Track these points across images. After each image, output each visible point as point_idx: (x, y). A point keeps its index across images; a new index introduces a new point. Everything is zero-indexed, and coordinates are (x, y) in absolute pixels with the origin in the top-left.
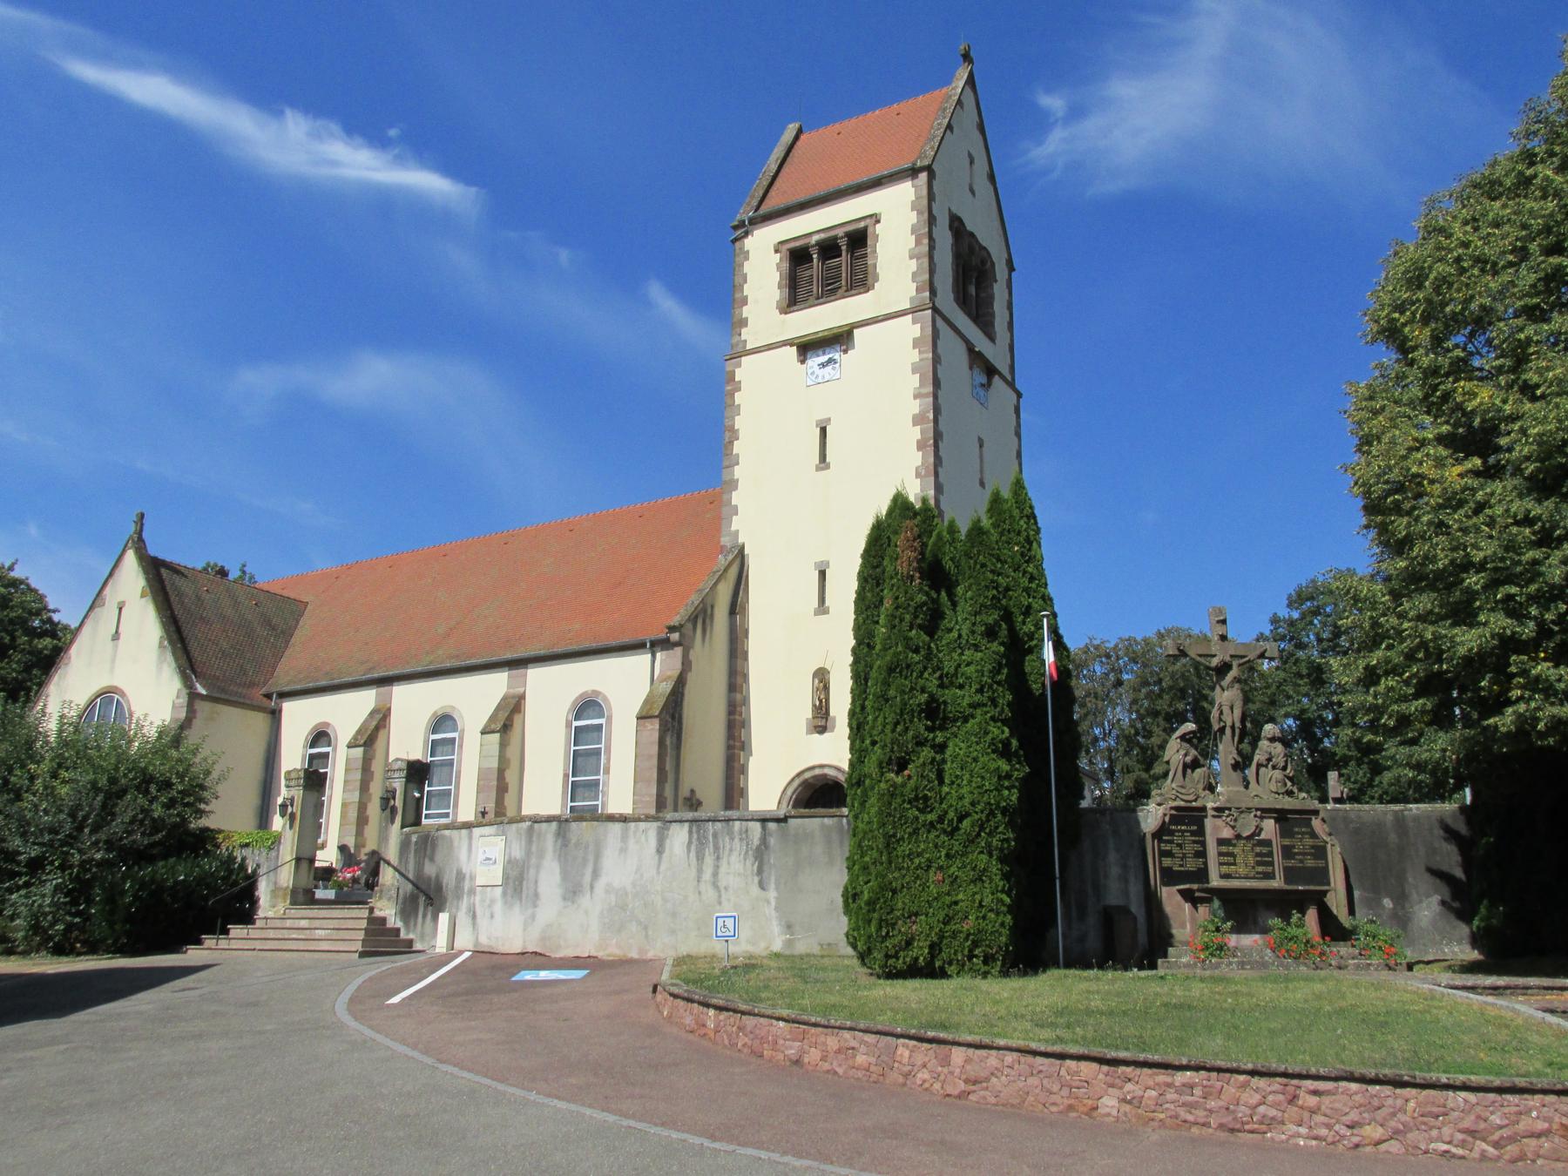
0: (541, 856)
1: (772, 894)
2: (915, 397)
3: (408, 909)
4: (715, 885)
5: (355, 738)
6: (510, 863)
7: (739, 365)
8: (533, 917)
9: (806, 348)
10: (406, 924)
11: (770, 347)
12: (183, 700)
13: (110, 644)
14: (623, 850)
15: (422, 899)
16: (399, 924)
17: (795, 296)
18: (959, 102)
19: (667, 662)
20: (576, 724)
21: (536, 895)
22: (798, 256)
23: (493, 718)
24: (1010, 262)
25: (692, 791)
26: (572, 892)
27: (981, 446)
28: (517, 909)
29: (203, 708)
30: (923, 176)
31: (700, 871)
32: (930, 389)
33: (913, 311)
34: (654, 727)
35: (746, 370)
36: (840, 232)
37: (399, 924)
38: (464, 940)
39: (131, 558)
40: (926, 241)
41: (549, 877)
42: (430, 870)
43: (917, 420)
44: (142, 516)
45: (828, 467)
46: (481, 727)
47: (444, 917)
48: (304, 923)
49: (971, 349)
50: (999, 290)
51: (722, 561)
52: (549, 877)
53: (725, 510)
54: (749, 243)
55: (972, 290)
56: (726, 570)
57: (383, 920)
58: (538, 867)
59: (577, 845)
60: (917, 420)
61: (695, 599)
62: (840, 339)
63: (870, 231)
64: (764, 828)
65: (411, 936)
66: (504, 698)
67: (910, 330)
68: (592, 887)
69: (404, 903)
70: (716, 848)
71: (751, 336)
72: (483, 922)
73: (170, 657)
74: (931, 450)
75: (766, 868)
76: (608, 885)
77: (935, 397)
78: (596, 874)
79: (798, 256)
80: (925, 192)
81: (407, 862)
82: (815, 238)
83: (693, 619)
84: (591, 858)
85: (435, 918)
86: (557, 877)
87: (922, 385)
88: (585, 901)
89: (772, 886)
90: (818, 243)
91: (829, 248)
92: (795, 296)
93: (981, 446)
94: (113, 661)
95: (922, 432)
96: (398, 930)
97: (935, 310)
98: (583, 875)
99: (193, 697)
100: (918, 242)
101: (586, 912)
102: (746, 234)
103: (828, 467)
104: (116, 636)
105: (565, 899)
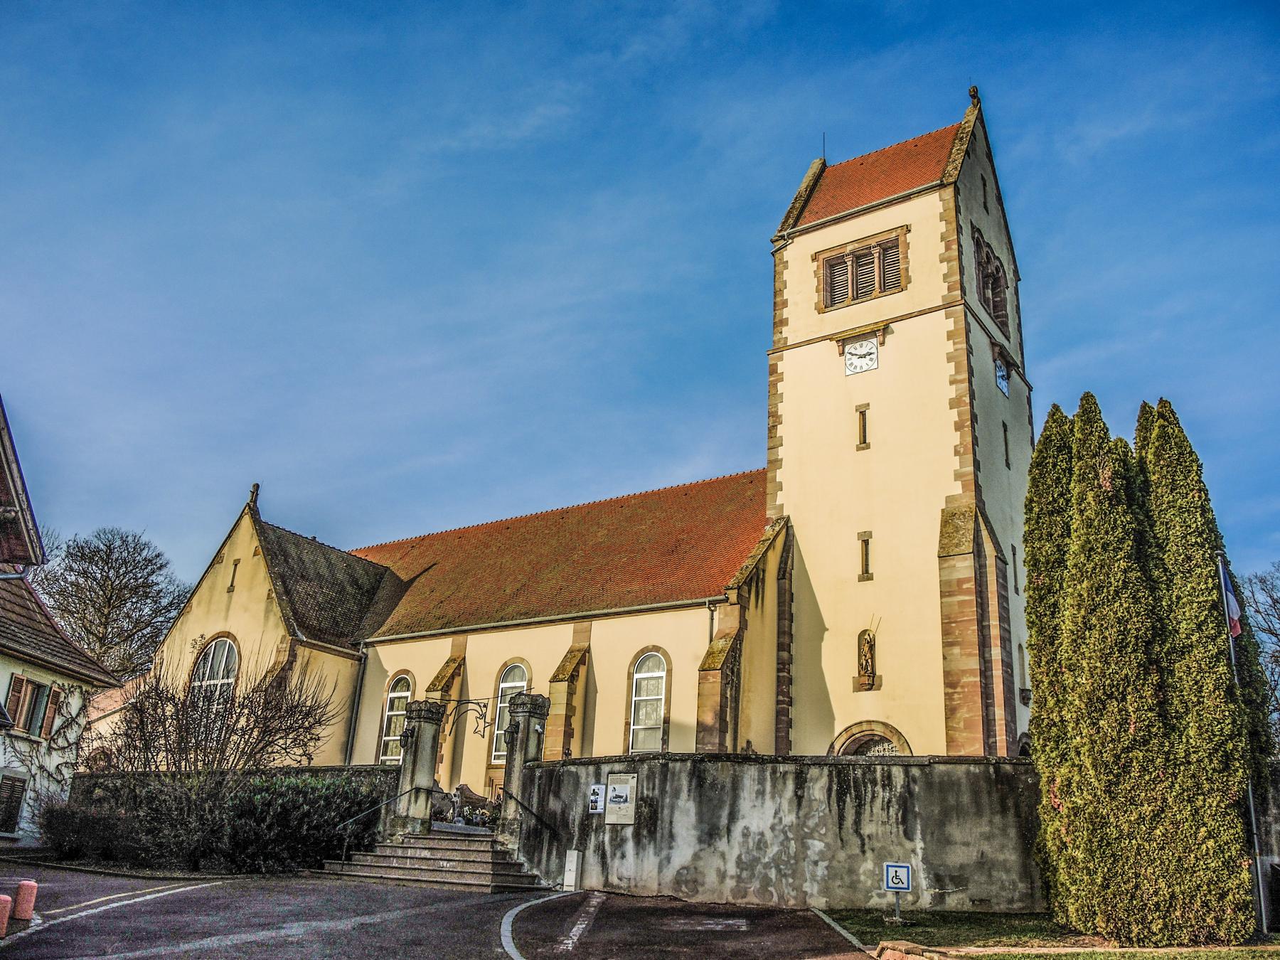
0: (676, 794)
1: (919, 845)
2: (952, 383)
3: (532, 841)
4: (857, 831)
5: (433, 684)
6: (641, 800)
7: (781, 359)
8: (668, 859)
9: (843, 341)
10: (530, 860)
11: (809, 342)
12: (286, 646)
13: (226, 595)
14: (761, 793)
15: (546, 836)
16: (522, 859)
17: (831, 298)
18: (973, 134)
19: (727, 619)
20: (502, 685)
21: (672, 836)
22: (831, 264)
23: (561, 669)
24: (1016, 272)
25: (749, 742)
26: (710, 834)
27: (1005, 431)
28: (651, 850)
29: (303, 653)
30: (950, 190)
31: (841, 818)
32: (965, 376)
33: (947, 306)
34: (715, 678)
35: (788, 363)
36: (873, 242)
37: (522, 859)
38: (594, 880)
39: (247, 521)
40: (955, 247)
41: (684, 817)
42: (554, 805)
43: (954, 404)
44: (257, 487)
45: (868, 447)
46: (550, 676)
47: (572, 857)
48: (426, 854)
49: (994, 344)
50: (1009, 294)
51: (769, 531)
52: (684, 817)
53: (770, 487)
54: (788, 254)
55: (989, 293)
56: (774, 539)
57: (506, 853)
58: (672, 808)
59: (713, 785)
60: (954, 404)
61: (749, 563)
62: (882, 330)
63: (901, 239)
64: (907, 773)
65: (535, 872)
66: (571, 651)
67: (943, 323)
68: (729, 831)
69: (528, 838)
70: (858, 797)
71: (790, 333)
72: (615, 864)
73: (276, 608)
74: (968, 430)
75: (910, 816)
76: (746, 828)
77: (970, 383)
78: (733, 817)
79: (831, 264)
80: (952, 204)
81: (530, 797)
82: (850, 248)
83: (748, 582)
84: (728, 800)
85: (562, 857)
86: (693, 818)
87: (957, 372)
88: (722, 845)
89: (918, 835)
90: (852, 253)
91: (860, 257)
92: (831, 298)
93: (1005, 431)
94: (228, 609)
95: (959, 414)
96: (522, 865)
97: (966, 305)
98: (720, 817)
99: (296, 642)
100: (948, 248)
101: (723, 856)
102: (785, 246)
103: (868, 447)
104: (231, 589)
105: (700, 841)
